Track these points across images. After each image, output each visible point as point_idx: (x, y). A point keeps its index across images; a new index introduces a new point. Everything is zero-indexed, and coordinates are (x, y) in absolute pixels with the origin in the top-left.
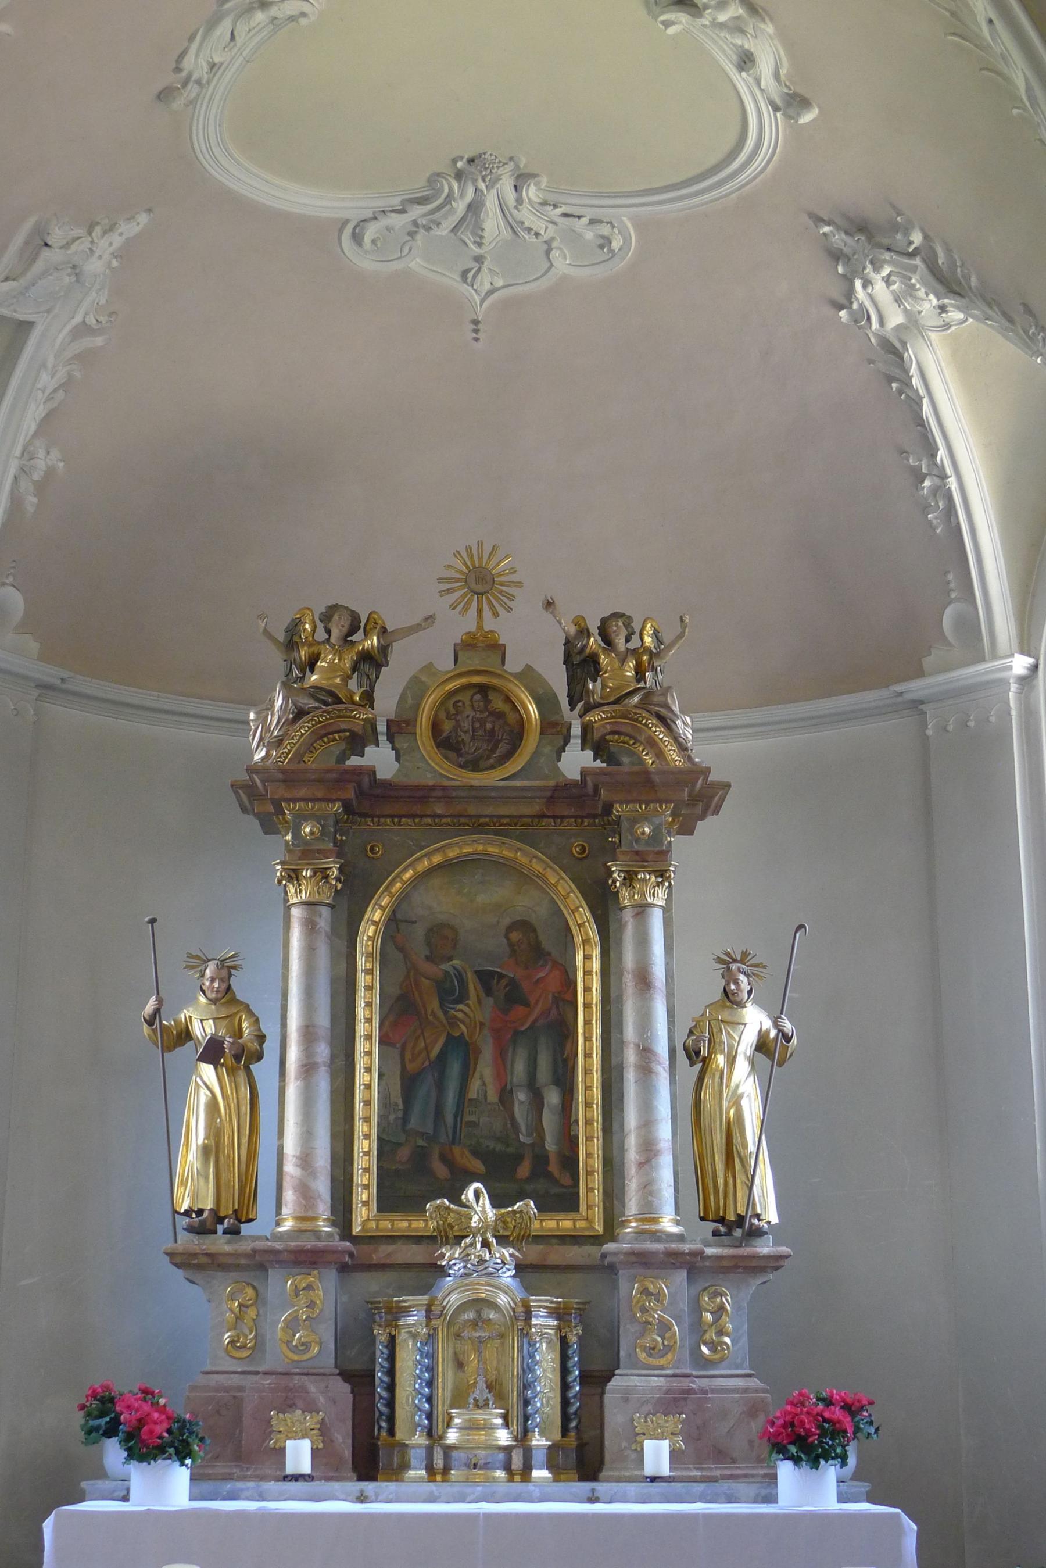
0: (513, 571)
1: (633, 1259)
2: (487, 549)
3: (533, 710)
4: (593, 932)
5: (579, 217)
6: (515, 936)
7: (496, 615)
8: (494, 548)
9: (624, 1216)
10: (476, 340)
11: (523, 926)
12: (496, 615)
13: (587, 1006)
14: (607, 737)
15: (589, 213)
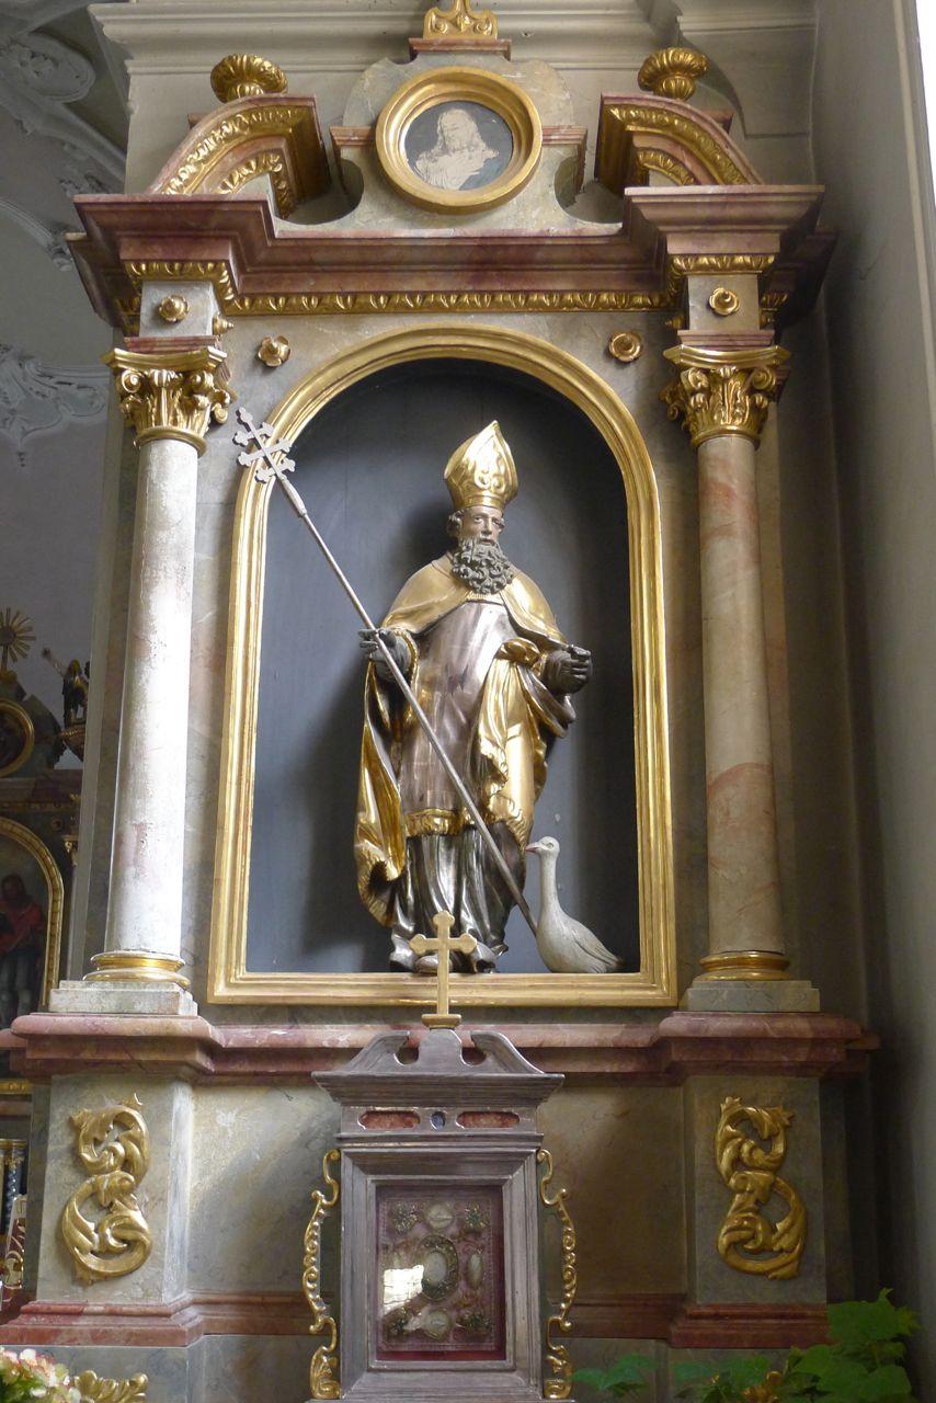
0: (30, 629)
1: (130, 961)
2: (13, 614)
3: (31, 727)
4: (60, 881)
5: (70, 384)
6: (8, 886)
7: (15, 660)
8: (18, 613)
9: (119, 948)
10: (23, 465)
11: (15, 879)
12: (15, 660)
13: (52, 936)
14: (411, 40)
15: (76, 382)
